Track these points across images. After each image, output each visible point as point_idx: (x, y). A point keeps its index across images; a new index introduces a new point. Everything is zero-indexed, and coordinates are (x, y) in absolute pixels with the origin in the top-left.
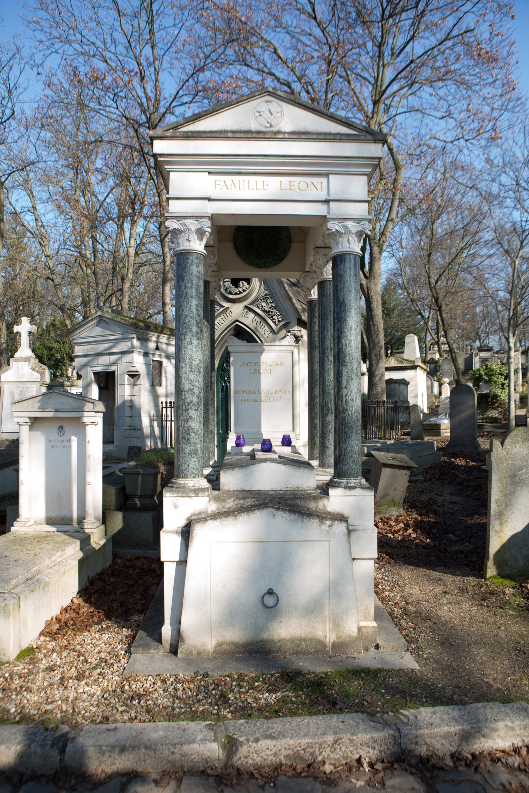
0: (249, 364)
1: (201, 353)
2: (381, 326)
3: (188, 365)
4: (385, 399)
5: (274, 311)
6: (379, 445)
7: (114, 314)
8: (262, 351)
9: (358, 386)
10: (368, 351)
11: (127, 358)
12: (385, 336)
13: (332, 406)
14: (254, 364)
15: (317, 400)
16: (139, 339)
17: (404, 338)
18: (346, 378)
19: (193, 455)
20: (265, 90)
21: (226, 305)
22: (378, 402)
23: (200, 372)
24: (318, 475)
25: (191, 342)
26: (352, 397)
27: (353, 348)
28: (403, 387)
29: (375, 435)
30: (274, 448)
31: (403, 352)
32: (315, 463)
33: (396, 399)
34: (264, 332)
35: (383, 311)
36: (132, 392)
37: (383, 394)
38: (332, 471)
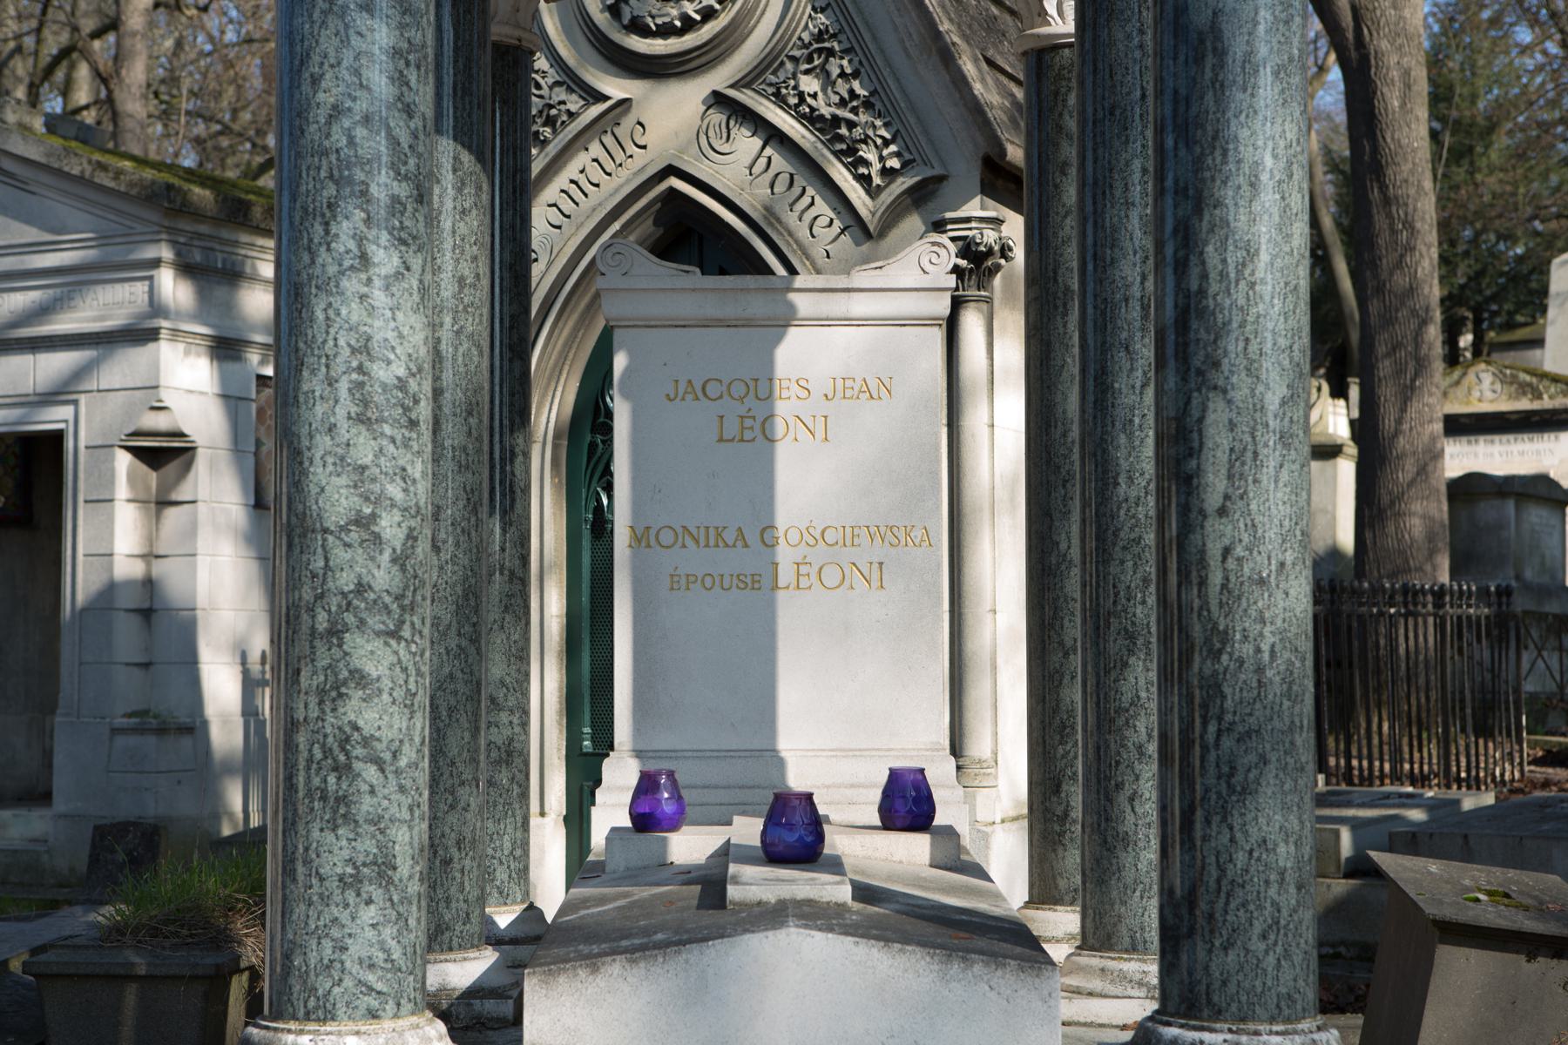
0: (712, 389)
1: (418, 321)
2: (1425, 208)
3: (343, 386)
4: (1444, 578)
5: (863, 117)
6: (1417, 815)
7: (56, 142)
8: (784, 320)
9: (1295, 500)
10: (1355, 336)
11: (124, 367)
12: (1444, 260)
13: (1145, 612)
14: (738, 389)
15: (1073, 584)
16: (186, 269)
17: (1543, 270)
18: (1223, 456)
19: (370, 889)
21: (615, 87)
22: (1411, 595)
23: (413, 424)
24: (1077, 992)
25: (364, 258)
26: (1261, 563)
27: (1266, 290)
28: (1537, 515)
29: (1396, 760)
30: (837, 842)
31: (1538, 342)
32: (1059, 926)
33: (1506, 577)
34: (813, 222)
35: (1434, 135)
36: (151, 538)
37: (1432, 553)
38: (1151, 969)
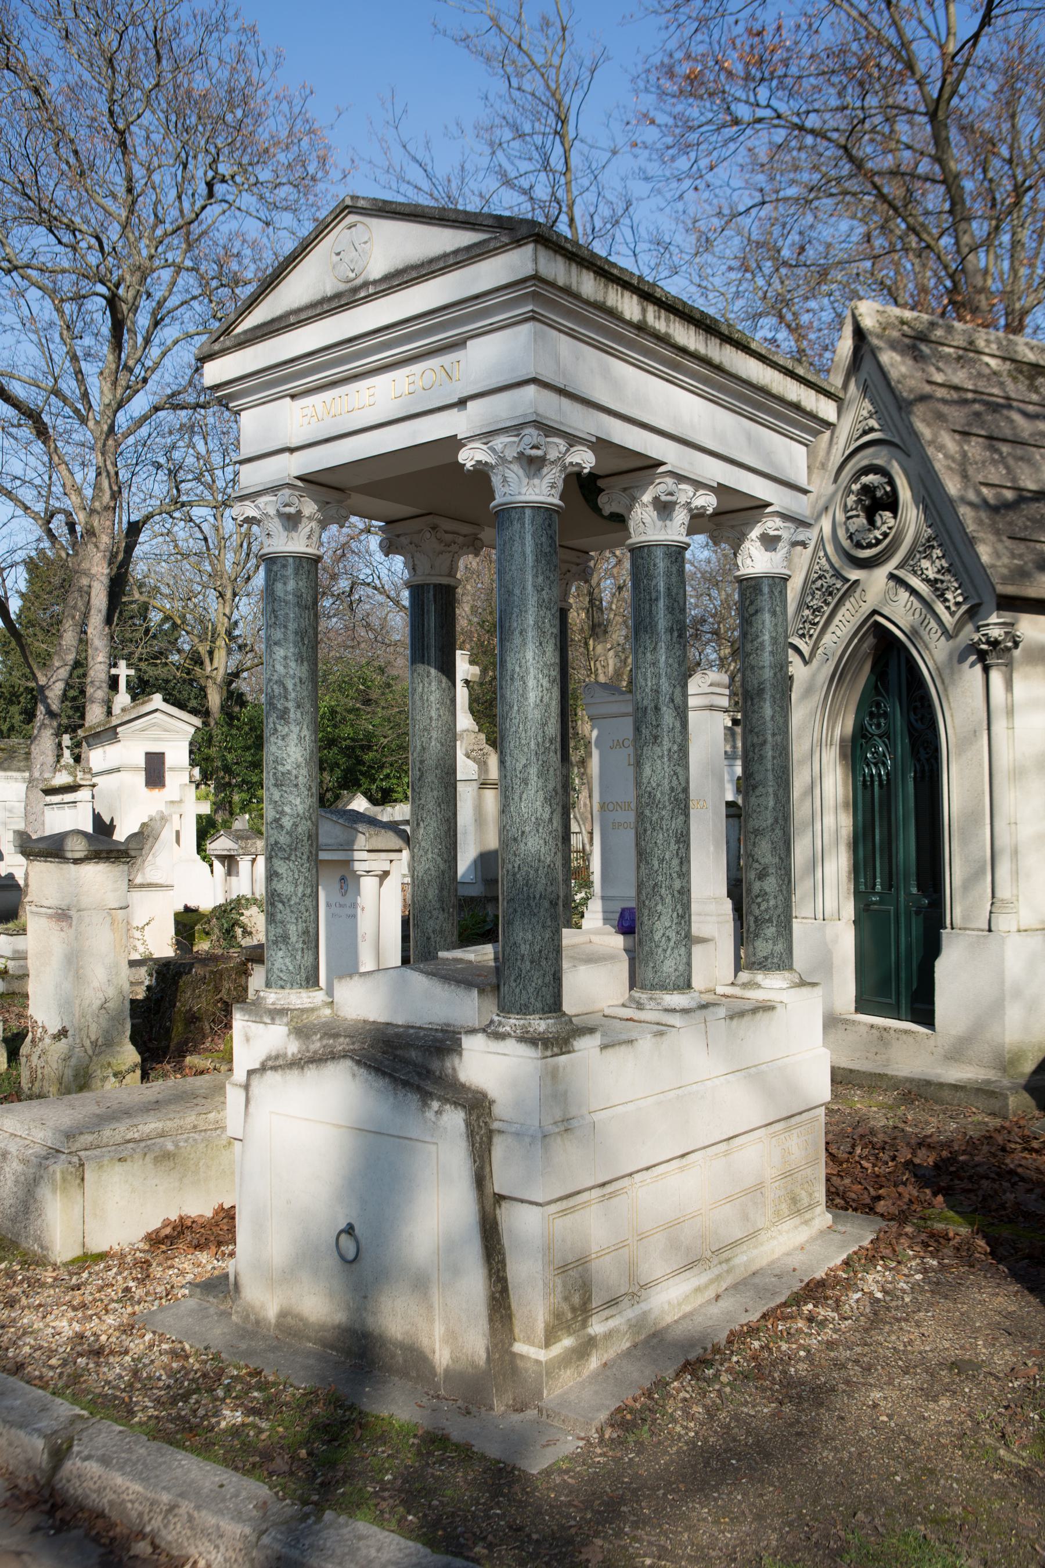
19: (281, 945)
20: (342, 207)
21: (854, 575)
25: (276, 730)
